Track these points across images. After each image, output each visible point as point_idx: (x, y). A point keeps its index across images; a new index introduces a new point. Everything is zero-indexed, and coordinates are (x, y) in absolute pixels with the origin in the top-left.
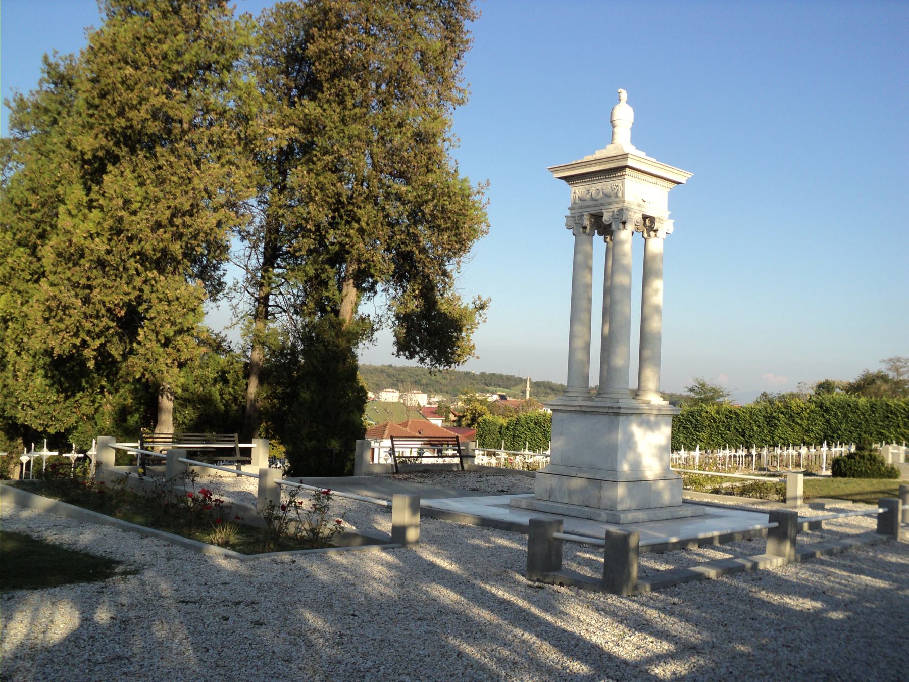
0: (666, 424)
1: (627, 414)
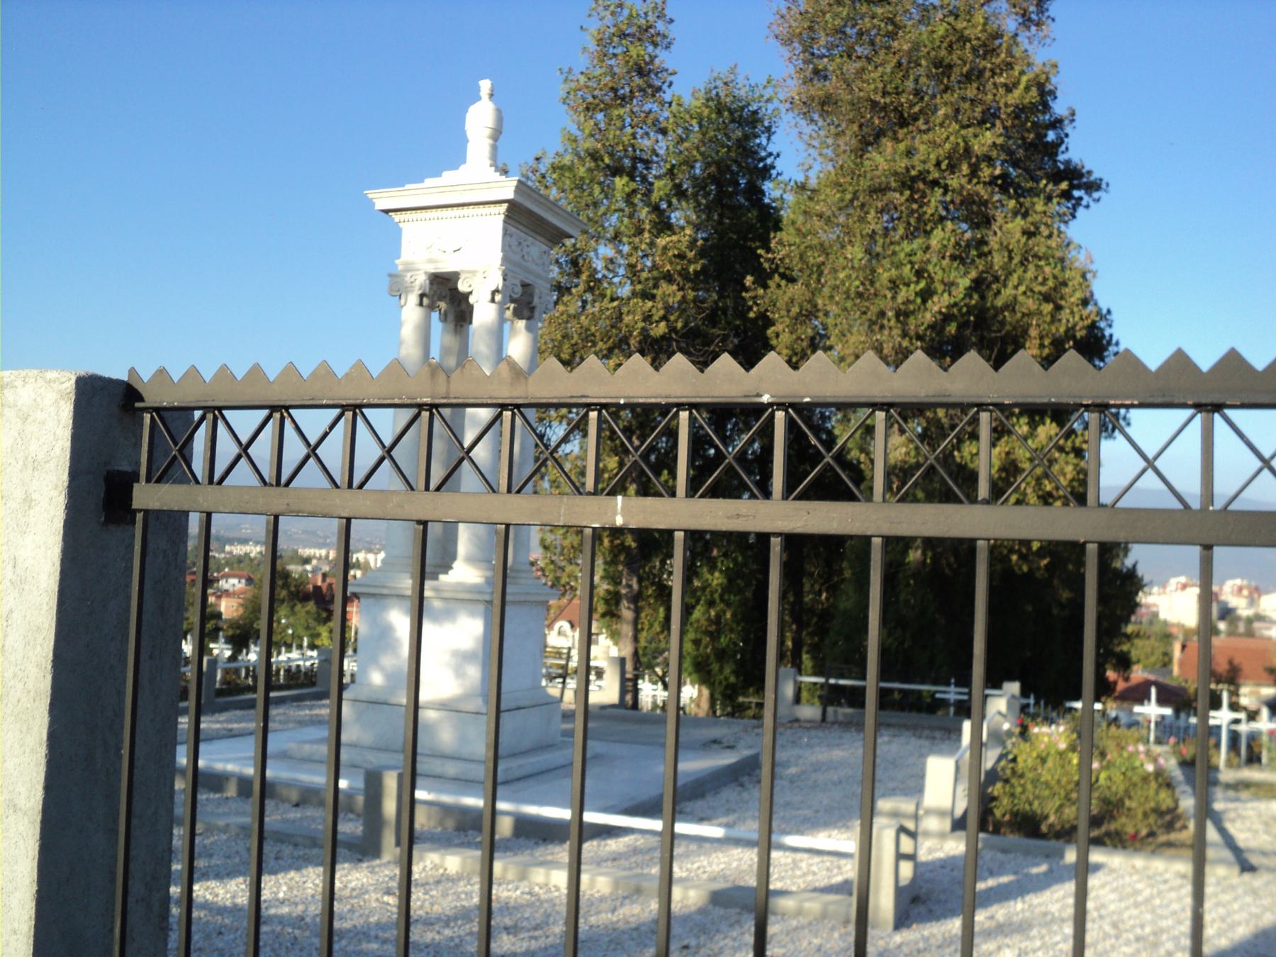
0: (473, 614)
1: (373, 595)
